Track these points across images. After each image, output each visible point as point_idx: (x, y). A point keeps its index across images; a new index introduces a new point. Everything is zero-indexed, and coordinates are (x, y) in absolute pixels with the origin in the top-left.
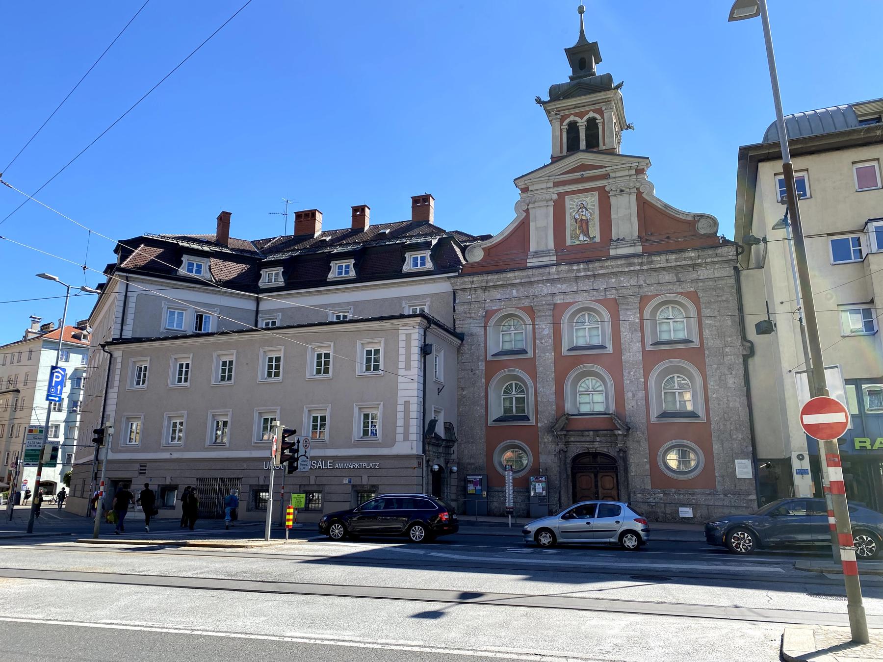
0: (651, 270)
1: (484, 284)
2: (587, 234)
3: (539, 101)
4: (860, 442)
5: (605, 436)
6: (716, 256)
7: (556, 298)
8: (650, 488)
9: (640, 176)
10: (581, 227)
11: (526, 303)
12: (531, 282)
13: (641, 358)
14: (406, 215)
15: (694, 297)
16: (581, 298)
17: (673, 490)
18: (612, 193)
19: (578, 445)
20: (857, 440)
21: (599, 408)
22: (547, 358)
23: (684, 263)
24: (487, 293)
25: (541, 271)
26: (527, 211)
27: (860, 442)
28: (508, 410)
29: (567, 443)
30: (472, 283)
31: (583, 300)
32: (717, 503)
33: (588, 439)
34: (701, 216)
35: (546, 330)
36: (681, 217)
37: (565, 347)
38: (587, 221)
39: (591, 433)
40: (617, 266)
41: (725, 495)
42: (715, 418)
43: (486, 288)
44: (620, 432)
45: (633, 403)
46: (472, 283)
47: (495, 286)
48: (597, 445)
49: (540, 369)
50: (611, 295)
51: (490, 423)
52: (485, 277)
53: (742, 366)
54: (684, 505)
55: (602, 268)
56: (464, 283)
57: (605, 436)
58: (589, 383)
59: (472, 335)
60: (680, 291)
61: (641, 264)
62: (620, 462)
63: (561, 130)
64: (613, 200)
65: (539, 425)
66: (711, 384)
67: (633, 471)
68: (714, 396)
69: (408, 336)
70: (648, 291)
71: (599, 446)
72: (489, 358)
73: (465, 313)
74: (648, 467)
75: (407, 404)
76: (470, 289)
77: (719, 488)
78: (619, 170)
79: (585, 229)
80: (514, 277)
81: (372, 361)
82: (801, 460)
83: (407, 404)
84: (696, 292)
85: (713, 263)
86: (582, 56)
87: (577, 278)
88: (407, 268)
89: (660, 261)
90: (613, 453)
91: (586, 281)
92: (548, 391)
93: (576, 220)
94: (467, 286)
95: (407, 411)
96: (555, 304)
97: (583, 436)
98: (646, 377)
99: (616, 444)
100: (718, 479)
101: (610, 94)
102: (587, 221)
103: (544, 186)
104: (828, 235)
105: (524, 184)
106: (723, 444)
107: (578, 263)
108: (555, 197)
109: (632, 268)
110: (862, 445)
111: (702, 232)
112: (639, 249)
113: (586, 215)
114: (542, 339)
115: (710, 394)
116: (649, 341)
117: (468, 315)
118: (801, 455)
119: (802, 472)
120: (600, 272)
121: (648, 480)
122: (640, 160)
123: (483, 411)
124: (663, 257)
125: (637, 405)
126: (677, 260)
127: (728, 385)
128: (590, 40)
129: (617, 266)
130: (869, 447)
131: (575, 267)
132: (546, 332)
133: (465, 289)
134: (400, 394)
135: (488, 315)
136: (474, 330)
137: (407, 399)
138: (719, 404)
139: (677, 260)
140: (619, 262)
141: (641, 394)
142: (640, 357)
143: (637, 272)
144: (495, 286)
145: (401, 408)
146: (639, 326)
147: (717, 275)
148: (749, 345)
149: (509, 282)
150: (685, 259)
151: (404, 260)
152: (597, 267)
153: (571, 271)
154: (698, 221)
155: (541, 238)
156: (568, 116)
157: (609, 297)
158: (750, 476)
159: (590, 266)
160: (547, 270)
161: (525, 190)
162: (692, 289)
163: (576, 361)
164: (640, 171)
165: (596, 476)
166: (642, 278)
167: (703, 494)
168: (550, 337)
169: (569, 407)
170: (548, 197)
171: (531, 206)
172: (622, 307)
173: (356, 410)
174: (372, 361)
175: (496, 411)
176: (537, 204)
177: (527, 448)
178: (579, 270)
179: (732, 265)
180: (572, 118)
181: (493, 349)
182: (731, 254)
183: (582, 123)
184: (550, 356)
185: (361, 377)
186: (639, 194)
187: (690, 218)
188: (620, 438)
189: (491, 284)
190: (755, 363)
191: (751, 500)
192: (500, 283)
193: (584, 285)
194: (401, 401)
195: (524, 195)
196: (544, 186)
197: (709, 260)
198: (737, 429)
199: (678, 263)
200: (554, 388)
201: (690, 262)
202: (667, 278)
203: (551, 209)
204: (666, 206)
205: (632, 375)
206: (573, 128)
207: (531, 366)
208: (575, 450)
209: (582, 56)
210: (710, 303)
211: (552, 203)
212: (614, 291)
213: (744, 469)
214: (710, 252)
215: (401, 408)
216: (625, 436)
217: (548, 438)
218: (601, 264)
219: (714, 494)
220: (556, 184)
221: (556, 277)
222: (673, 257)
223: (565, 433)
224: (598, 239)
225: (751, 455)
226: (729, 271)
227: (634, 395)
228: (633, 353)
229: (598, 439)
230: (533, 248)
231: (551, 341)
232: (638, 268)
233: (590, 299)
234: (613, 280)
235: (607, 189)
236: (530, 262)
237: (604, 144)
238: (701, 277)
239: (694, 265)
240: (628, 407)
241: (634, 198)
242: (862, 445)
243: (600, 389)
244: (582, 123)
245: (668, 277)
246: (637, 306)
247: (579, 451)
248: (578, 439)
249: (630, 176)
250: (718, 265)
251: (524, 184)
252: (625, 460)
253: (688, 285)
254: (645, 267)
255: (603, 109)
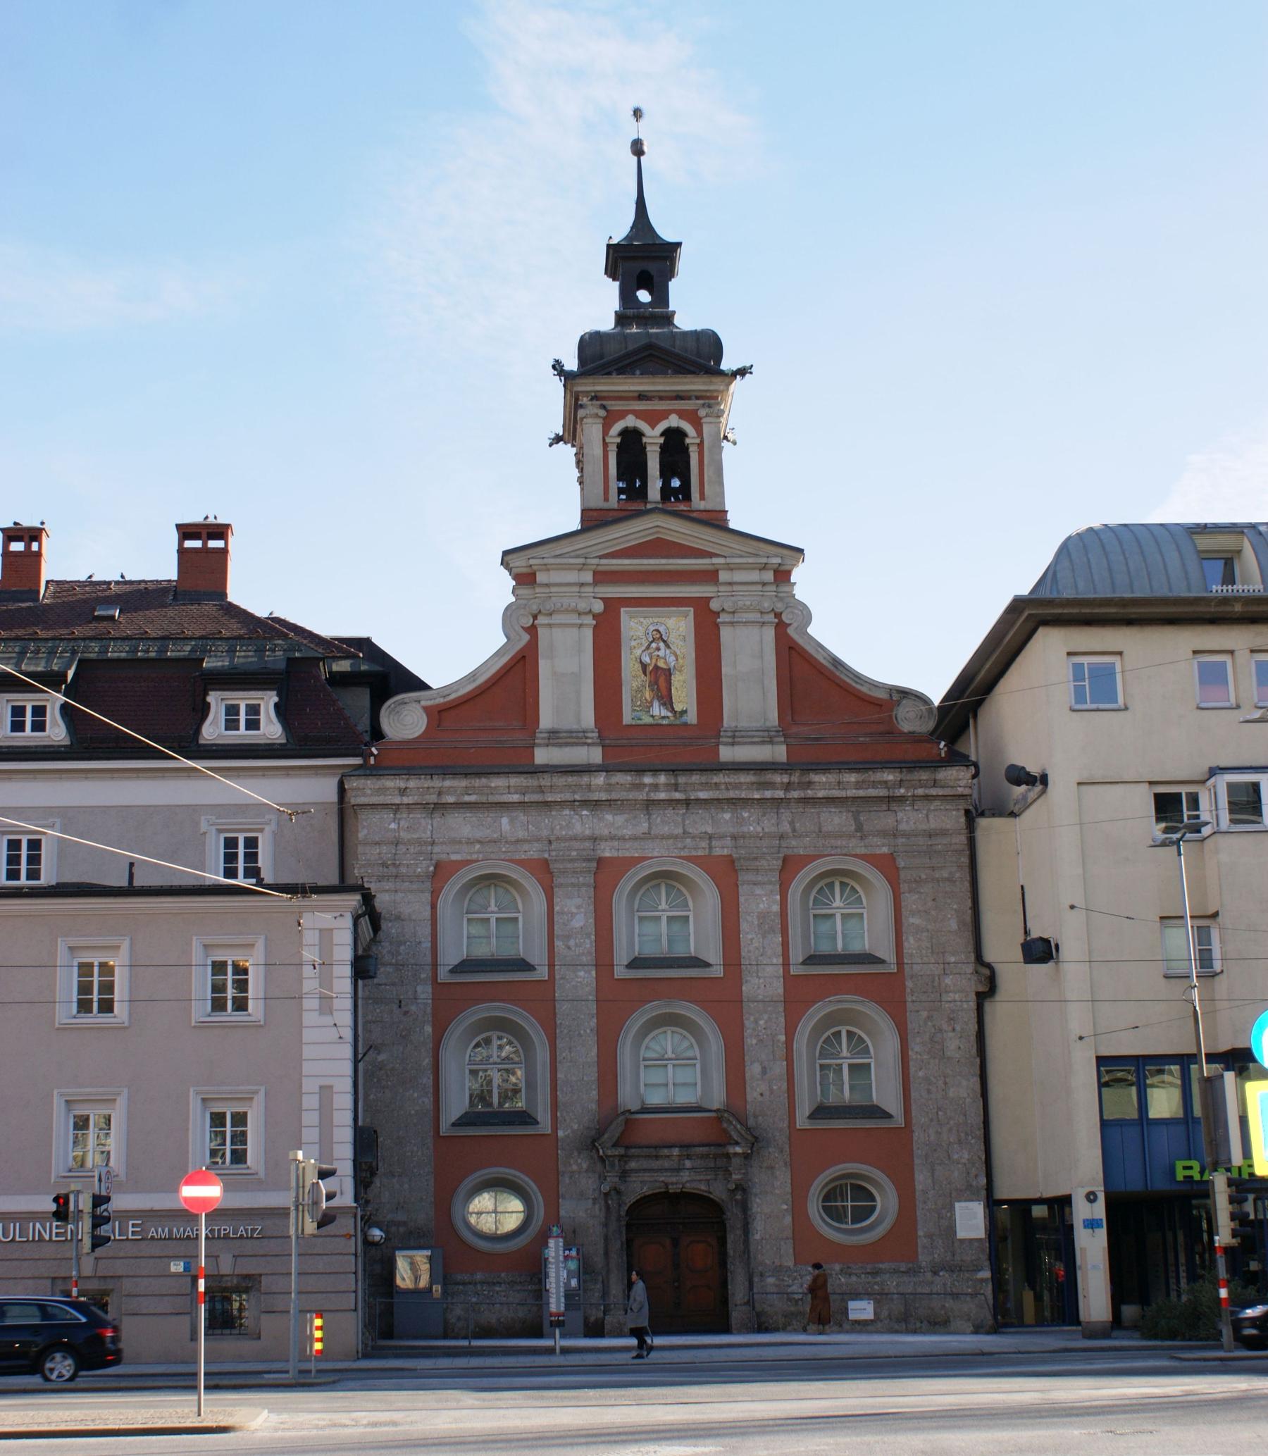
0: (805, 801)
1: (433, 798)
2: (667, 701)
3: (558, 367)
4: (1185, 1168)
5: (704, 1157)
6: (935, 783)
7: (603, 845)
8: (791, 1264)
9: (783, 588)
10: (654, 684)
11: (533, 851)
12: (546, 804)
13: (781, 991)
14: (159, 564)
15: (887, 866)
16: (655, 849)
17: (837, 1267)
18: (723, 618)
19: (647, 1177)
20: (1180, 1164)
21: (685, 1097)
22: (579, 982)
23: (872, 792)
24: (437, 820)
25: (571, 780)
26: (532, 630)
27: (1185, 1168)
28: (482, 1096)
29: (624, 1175)
30: (403, 792)
31: (661, 855)
32: (919, 1290)
33: (666, 1164)
34: (905, 693)
35: (576, 911)
36: (864, 689)
37: (621, 957)
38: (668, 673)
39: (676, 1151)
40: (737, 786)
41: (935, 1273)
42: (919, 1118)
43: (438, 808)
44: (738, 1150)
45: (763, 1087)
46: (403, 792)
47: (459, 806)
48: (685, 1176)
49: (563, 1008)
50: (722, 849)
51: (444, 1129)
52: (437, 783)
53: (974, 1015)
54: (857, 1296)
55: (706, 786)
56: (382, 791)
57: (704, 1157)
58: (668, 1041)
59: (398, 918)
60: (863, 851)
61: (788, 787)
62: (733, 1215)
63: (605, 445)
64: (726, 634)
65: (560, 1133)
66: (916, 1048)
67: (759, 1229)
68: (921, 1074)
69: (326, 934)
70: (799, 847)
71: (689, 1178)
72: (443, 976)
73: (384, 865)
74: (788, 1220)
75: (326, 1092)
76: (396, 808)
77: (924, 1259)
78: (740, 567)
79: (664, 692)
80: (503, 787)
81: (229, 991)
82: (1092, 1201)
83: (326, 1092)
84: (891, 857)
85: (927, 797)
86: (642, 261)
87: (649, 805)
88: (213, 730)
89: (823, 784)
90: (718, 1191)
91: (669, 812)
92: (581, 1055)
93: (644, 667)
94: (389, 800)
95: (326, 1110)
96: (600, 861)
97: (657, 1157)
98: (790, 1031)
99: (728, 1173)
100: (922, 1241)
101: (715, 384)
102: (668, 673)
103: (572, 577)
104: (1151, 783)
105: (524, 564)
106: (933, 1171)
107: (655, 771)
108: (599, 607)
109: (768, 794)
110: (1188, 1173)
111: (906, 727)
112: (780, 752)
113: (666, 658)
114: (568, 937)
115: (912, 1070)
116: (797, 955)
117: (393, 870)
118: (1093, 1193)
119: (1091, 1224)
120: (702, 795)
121: (787, 1248)
122: (785, 552)
123: (428, 1102)
124: (831, 778)
125: (772, 1091)
126: (858, 785)
127: (948, 1054)
128: (667, 233)
129: (737, 786)
130: (1197, 1177)
131: (648, 780)
132: (578, 922)
133: (385, 806)
134: (307, 1068)
135: (441, 873)
136: (406, 910)
137: (327, 1082)
138: (929, 1092)
139: (858, 785)
140: (745, 778)
141: (779, 1068)
142: (778, 988)
143: (777, 802)
144: (459, 806)
145: (311, 1101)
146: (778, 921)
147: (933, 824)
148: (987, 972)
149: (492, 799)
150: (874, 785)
151: (203, 711)
152: (698, 787)
153: (639, 787)
154: (899, 703)
155: (565, 696)
156: (622, 415)
157: (717, 852)
158: (980, 1233)
159: (682, 780)
160: (585, 779)
161: (524, 580)
162: (885, 850)
163: (642, 991)
164: (783, 576)
165: (675, 1242)
166: (786, 815)
167: (896, 1271)
168: (588, 935)
169: (627, 1097)
170: (583, 606)
171: (541, 620)
172: (743, 877)
173: (194, 1104)
174: (229, 991)
175: (456, 1104)
176: (557, 619)
177: (532, 1187)
178: (655, 787)
179: (963, 805)
180: (630, 421)
181: (450, 956)
182: (962, 783)
183: (653, 436)
184: (585, 979)
185: (203, 1026)
186: (781, 627)
187: (882, 695)
188: (736, 1161)
189: (451, 799)
190: (998, 1011)
191: (982, 1280)
192: (472, 798)
193: (667, 823)
194: (310, 1085)
195: (525, 591)
196: (572, 577)
197: (920, 792)
198: (960, 1142)
199: (861, 793)
200: (595, 1050)
201: (882, 792)
202: (837, 820)
203: (589, 633)
204: (837, 662)
205: (763, 1024)
206: (631, 444)
207: (542, 999)
208: (639, 1187)
209: (642, 261)
210: (918, 881)
211: (589, 620)
212: (728, 842)
213: (971, 1221)
214: (924, 775)
215: (311, 1101)
216: (747, 1157)
217: (581, 1163)
218: (704, 779)
219: (913, 1271)
220: (602, 577)
221: (604, 796)
222: (852, 778)
223: (621, 1151)
224: (692, 718)
225: (984, 1193)
226: (953, 819)
227: (764, 1071)
228: (763, 983)
229: (688, 1164)
230: (546, 720)
231: (589, 944)
232: (780, 794)
233: (676, 853)
234: (727, 816)
235: (714, 605)
236: (542, 756)
237: (702, 497)
238: (903, 827)
239: (890, 799)
240: (752, 1095)
241: (769, 634)
242: (1188, 1173)
243: (690, 1054)
244: (653, 436)
245: (836, 820)
246: (775, 877)
247: (646, 1190)
248: (645, 1164)
249: (764, 584)
250: (937, 803)
251: (524, 564)
252: (745, 1207)
253: (877, 840)
254: (795, 794)
255: (702, 413)
